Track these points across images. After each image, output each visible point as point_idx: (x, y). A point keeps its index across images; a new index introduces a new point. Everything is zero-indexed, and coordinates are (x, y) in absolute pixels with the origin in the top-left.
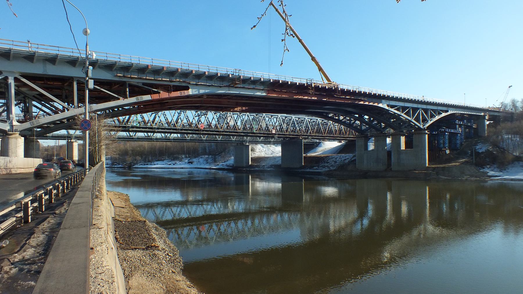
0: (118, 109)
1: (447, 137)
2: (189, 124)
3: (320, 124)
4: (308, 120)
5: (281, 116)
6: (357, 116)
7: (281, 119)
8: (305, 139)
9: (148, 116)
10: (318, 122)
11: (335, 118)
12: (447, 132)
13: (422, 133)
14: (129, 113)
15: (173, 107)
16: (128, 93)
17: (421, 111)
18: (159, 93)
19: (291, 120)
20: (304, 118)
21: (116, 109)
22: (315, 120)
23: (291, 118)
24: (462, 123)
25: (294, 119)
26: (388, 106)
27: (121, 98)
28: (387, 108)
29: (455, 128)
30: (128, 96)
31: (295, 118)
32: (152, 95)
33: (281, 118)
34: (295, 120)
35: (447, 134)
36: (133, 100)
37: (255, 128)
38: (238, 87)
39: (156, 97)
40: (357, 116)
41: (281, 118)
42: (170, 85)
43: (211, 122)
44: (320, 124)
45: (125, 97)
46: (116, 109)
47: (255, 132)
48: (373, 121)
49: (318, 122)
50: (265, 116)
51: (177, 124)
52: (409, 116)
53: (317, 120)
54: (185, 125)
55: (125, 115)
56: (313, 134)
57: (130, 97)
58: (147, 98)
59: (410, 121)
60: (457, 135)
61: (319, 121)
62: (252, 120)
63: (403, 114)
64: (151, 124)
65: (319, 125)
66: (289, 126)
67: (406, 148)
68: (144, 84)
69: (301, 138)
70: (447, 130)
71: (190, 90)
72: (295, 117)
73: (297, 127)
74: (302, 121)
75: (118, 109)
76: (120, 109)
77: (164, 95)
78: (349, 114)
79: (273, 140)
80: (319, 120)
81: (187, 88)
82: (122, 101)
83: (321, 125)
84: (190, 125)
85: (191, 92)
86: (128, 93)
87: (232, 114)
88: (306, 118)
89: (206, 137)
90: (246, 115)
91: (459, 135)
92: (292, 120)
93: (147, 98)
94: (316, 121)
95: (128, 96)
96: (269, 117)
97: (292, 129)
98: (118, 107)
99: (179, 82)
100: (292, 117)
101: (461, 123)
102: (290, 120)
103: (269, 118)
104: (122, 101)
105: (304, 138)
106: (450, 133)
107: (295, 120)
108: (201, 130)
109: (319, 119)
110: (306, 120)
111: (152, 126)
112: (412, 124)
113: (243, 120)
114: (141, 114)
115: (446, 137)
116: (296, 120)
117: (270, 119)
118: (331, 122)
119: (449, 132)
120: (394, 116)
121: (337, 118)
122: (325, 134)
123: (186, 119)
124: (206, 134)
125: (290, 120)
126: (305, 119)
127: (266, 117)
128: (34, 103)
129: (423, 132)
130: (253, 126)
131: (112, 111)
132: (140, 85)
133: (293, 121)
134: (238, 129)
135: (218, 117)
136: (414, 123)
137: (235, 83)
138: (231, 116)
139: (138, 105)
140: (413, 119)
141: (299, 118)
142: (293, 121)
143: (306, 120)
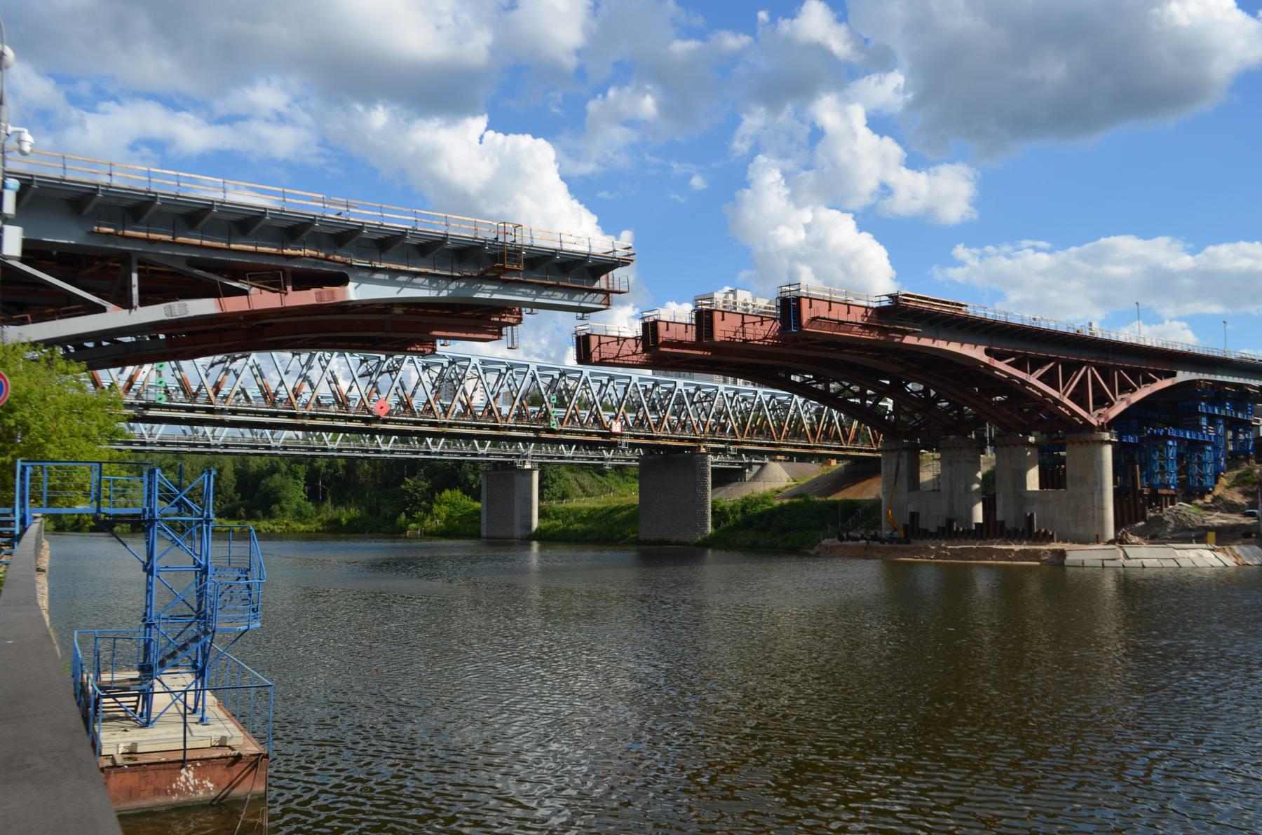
0: (98, 344)
1: (1172, 453)
2: (401, 398)
3: (765, 406)
4: (727, 395)
5: (592, 374)
6: (888, 382)
7: (640, 389)
8: (715, 452)
9: (197, 370)
10: (757, 400)
11: (814, 386)
12: (1172, 438)
13: (1087, 442)
14: (137, 355)
15: (293, 340)
16: (135, 291)
17: (1089, 372)
18: (245, 293)
19: (673, 393)
20: (671, 382)
21: (90, 345)
22: (750, 394)
23: (671, 386)
24: (1219, 411)
25: (681, 390)
26: (988, 352)
27: (110, 306)
28: (985, 359)
29: (1198, 428)
30: (135, 301)
31: (687, 388)
32: (221, 299)
33: (641, 386)
34: (684, 393)
35: (1170, 443)
36: (156, 313)
37: (555, 414)
38: (510, 281)
39: (234, 305)
40: (888, 382)
41: (641, 386)
42: (282, 269)
43: (470, 395)
44: (765, 406)
45: (125, 303)
46: (90, 345)
47: (555, 427)
48: (938, 398)
49: (757, 400)
50: (590, 379)
51: (296, 399)
52: (1052, 387)
53: (756, 393)
54: (323, 401)
55: (121, 363)
56: (743, 437)
57: (143, 303)
58: (204, 307)
59: (1058, 402)
60: (1204, 450)
61: (760, 398)
62: (545, 388)
63: (1033, 380)
64: (209, 398)
65: (760, 407)
66: (666, 412)
67: (1041, 486)
68: (192, 262)
69: (703, 450)
70: (1172, 432)
71: (351, 285)
72: (686, 384)
73: (691, 413)
74: (708, 395)
75: (98, 344)
76: (105, 344)
77: (262, 299)
78: (867, 376)
79: (611, 456)
80: (763, 393)
81: (342, 280)
82: (114, 317)
83: (769, 410)
84: (342, 401)
85: (354, 292)
86: (135, 291)
87: (481, 371)
88: (680, 383)
89: (339, 439)
90: (529, 373)
91: (1209, 448)
92: (676, 392)
93: (204, 307)
94: (751, 398)
95: (135, 301)
96: (601, 381)
97: (673, 420)
98: (97, 336)
99: (314, 260)
100: (675, 383)
101: (1216, 411)
102: (671, 391)
103: (602, 385)
104: (114, 317)
105: (713, 449)
106: (1180, 441)
107: (684, 393)
108: (377, 419)
109: (760, 391)
110: (722, 394)
111: (212, 404)
112: (1063, 409)
113: (519, 390)
114: (173, 363)
115: (1170, 455)
116: (688, 394)
117: (604, 388)
118: (800, 401)
119: (1178, 439)
120: (1007, 385)
121: (820, 386)
122: (779, 439)
123: (329, 383)
124: (337, 430)
125: (671, 391)
126: (717, 390)
127: (593, 381)
128: (435, 333)
129: (1096, 436)
130: (551, 410)
131: (75, 350)
132: (182, 267)
133: (680, 397)
134: (498, 418)
135: (433, 381)
136: (1068, 408)
137: (503, 268)
138: (479, 377)
139: (169, 331)
140: (1064, 394)
141: (698, 388)
142: (680, 397)
143: (719, 392)
